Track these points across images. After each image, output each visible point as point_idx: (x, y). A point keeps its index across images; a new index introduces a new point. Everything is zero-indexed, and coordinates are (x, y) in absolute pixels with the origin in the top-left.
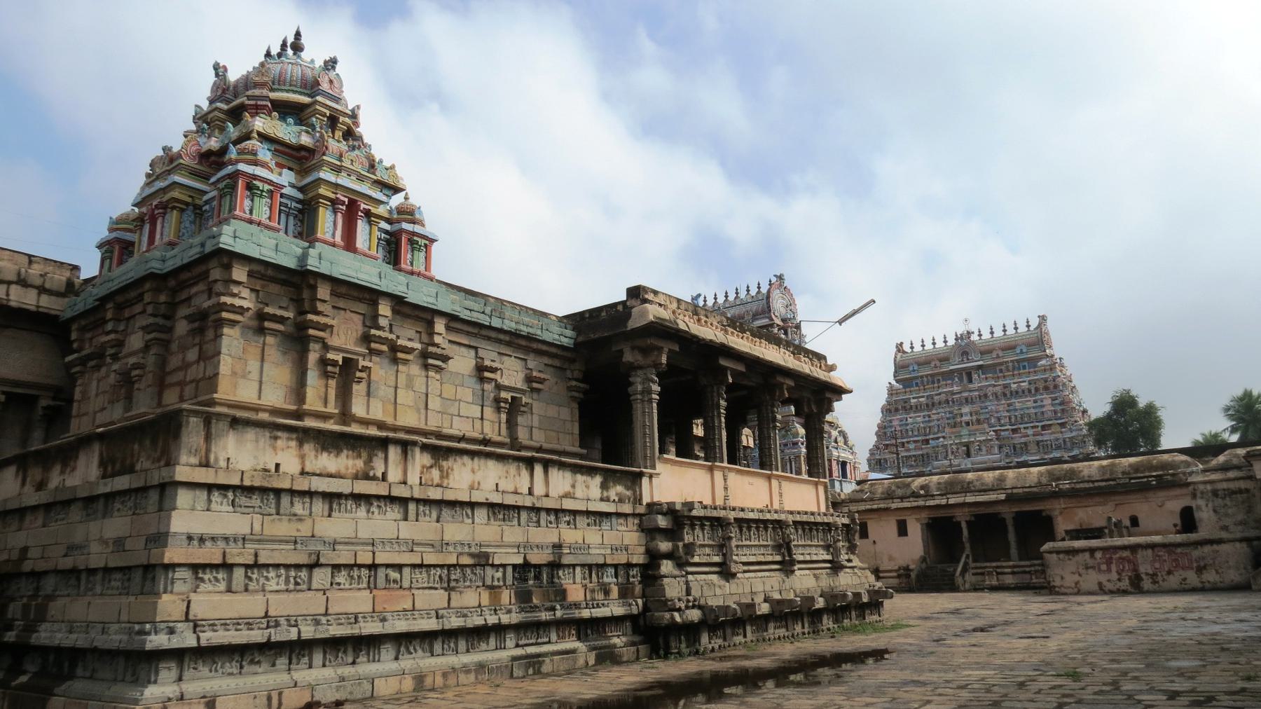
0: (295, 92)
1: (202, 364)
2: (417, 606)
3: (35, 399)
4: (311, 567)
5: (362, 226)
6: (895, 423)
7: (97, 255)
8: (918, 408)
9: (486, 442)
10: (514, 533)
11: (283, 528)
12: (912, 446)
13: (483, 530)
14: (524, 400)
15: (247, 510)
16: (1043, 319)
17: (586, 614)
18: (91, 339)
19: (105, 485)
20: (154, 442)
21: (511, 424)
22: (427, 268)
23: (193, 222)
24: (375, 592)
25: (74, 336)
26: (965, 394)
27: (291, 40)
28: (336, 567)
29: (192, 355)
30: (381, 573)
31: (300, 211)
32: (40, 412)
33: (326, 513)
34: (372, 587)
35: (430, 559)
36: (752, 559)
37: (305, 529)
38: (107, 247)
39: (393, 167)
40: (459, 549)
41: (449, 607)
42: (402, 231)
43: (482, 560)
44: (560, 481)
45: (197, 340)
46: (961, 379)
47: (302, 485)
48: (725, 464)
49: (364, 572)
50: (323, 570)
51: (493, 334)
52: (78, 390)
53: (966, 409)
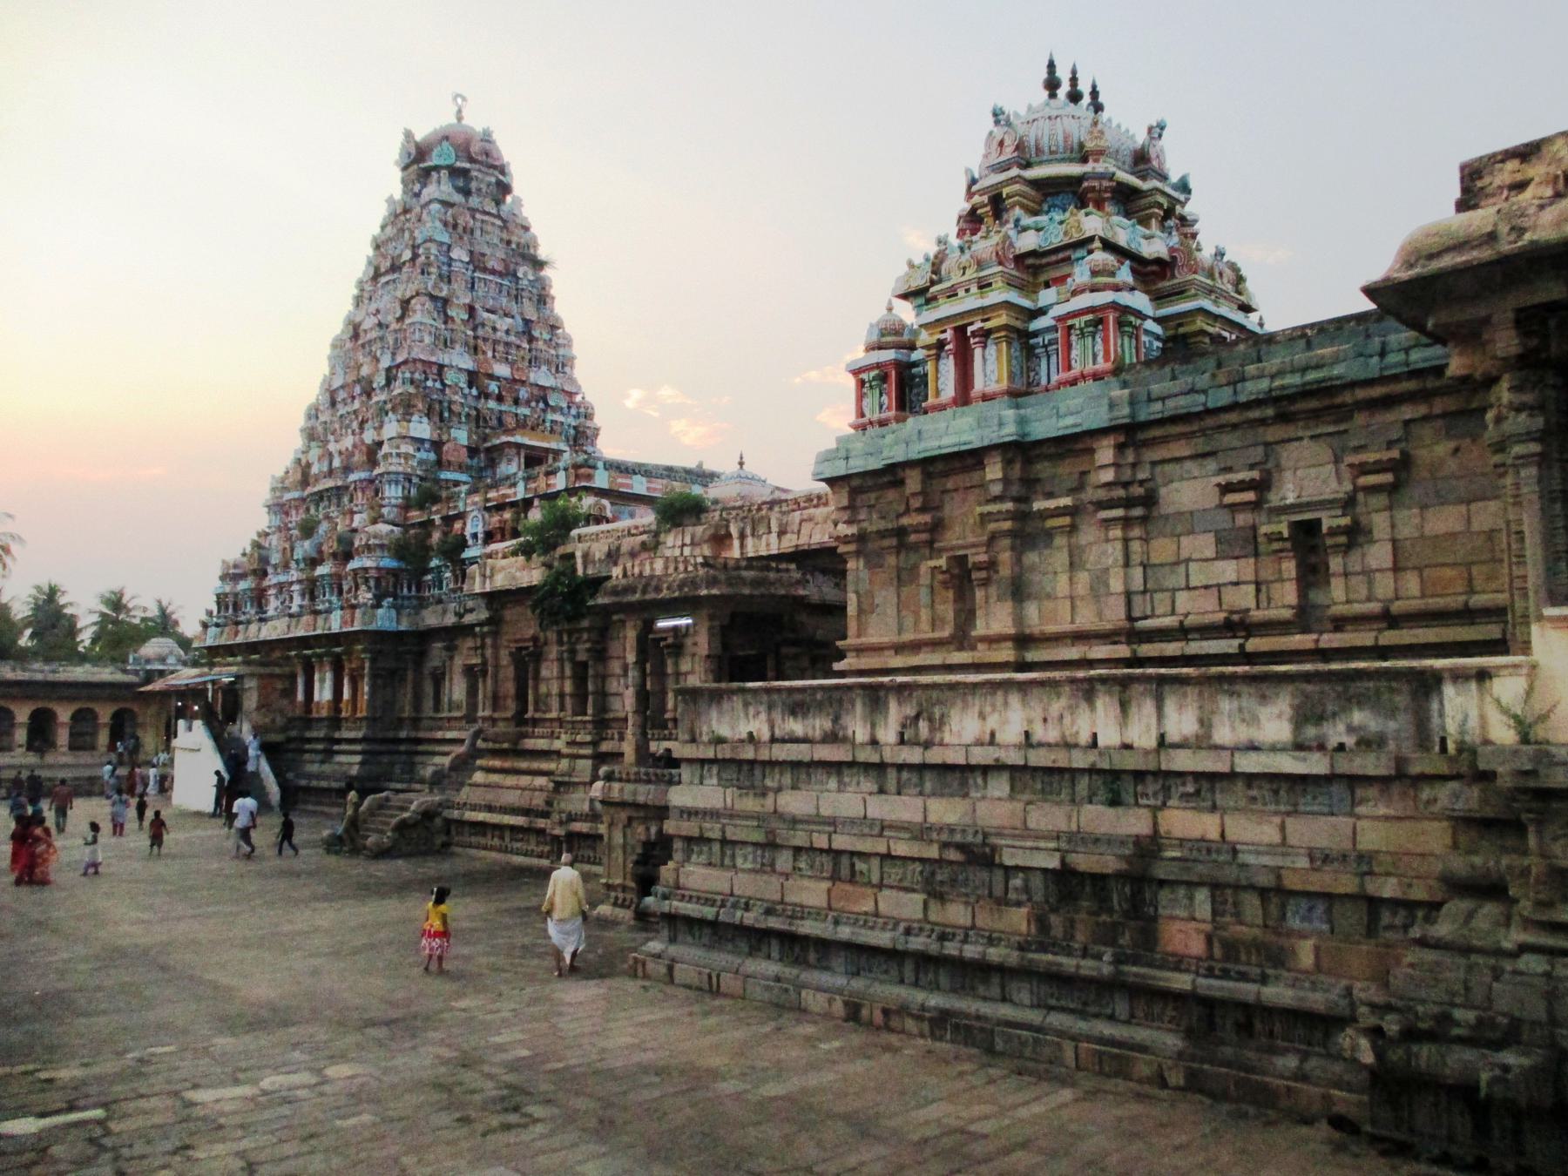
9: (1390, 620)
10: (1049, 817)
11: (750, 804)
20: (1200, 694)
28: (798, 850)
33: (696, 781)
34: (835, 877)
35: (901, 849)
40: (945, 837)
49: (825, 859)
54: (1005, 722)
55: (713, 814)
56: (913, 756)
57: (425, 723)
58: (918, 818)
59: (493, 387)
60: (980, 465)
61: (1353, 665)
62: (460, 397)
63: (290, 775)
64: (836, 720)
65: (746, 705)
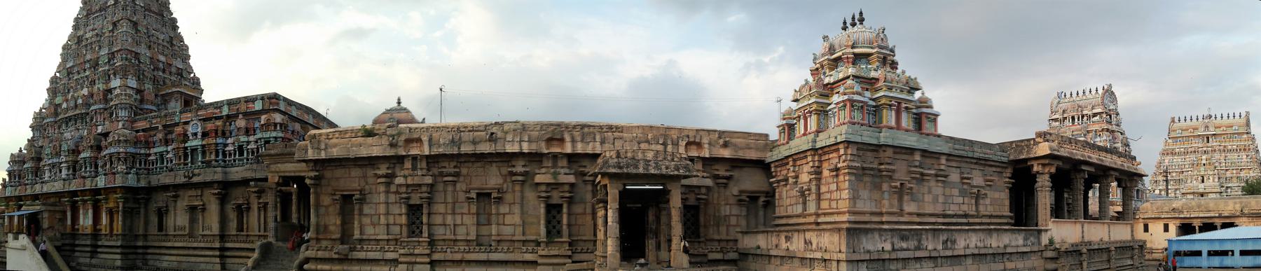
5: (904, 116)
7: (777, 130)
9: (966, 216)
14: (983, 192)
21: (977, 204)
27: (857, 17)
29: (833, 187)
38: (782, 128)
47: (894, 256)
56: (949, 253)
57: (150, 238)
59: (161, 65)
62: (147, 69)
63: (74, 264)
64: (919, 241)
65: (881, 236)
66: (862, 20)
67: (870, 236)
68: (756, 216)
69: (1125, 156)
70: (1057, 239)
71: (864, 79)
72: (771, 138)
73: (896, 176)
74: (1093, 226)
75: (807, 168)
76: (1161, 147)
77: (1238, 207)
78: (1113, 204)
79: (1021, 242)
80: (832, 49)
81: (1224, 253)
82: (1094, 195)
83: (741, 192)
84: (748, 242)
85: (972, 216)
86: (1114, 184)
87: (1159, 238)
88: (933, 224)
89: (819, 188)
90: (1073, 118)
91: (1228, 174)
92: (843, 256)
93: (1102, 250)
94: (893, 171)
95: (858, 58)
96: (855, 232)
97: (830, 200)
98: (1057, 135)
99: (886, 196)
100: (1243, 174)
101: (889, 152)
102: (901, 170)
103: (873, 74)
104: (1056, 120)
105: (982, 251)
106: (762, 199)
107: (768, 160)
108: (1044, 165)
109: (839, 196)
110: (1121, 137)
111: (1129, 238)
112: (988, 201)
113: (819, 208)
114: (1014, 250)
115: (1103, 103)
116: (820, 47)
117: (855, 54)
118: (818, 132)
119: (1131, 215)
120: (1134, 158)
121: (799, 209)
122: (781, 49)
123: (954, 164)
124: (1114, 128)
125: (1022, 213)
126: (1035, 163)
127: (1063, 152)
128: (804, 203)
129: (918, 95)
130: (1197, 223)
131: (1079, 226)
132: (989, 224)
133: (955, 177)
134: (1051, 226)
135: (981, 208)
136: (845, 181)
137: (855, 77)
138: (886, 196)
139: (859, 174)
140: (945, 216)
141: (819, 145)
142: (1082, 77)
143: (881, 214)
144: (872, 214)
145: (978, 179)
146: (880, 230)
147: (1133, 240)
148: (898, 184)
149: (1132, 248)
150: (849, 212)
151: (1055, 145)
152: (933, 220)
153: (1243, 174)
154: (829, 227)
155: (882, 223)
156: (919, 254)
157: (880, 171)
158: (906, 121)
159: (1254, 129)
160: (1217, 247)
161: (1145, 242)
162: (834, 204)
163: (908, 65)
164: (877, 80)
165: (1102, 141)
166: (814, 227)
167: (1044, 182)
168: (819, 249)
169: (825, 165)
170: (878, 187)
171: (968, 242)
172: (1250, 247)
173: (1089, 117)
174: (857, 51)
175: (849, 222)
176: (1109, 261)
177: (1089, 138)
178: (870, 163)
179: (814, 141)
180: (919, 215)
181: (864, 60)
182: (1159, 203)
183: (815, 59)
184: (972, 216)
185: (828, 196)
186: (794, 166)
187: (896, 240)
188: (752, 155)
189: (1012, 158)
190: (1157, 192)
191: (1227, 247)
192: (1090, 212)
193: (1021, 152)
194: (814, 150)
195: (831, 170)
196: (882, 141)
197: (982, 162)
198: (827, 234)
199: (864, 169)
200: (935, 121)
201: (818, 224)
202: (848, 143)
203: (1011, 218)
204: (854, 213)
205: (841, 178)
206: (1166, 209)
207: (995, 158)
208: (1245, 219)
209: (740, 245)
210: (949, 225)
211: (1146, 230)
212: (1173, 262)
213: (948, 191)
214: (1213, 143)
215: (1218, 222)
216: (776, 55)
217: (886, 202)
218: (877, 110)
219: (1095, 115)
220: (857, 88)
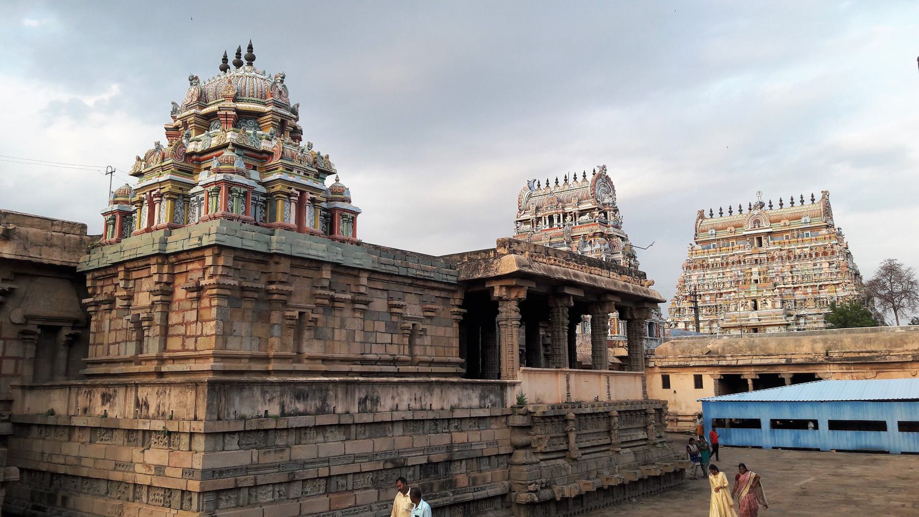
0: (253, 102)
1: (199, 323)
2: (358, 502)
3: (58, 329)
4: (290, 482)
5: (309, 211)
6: (694, 278)
7: (102, 220)
8: (714, 266)
9: (394, 362)
10: (421, 441)
11: (272, 458)
12: (707, 298)
13: (400, 440)
14: (421, 326)
15: (248, 447)
16: (825, 193)
17: (469, 496)
18: (102, 287)
19: (144, 423)
21: (411, 345)
22: (354, 235)
23: (183, 208)
24: (331, 496)
25: (89, 284)
26: (756, 257)
27: (244, 52)
29: (191, 316)
30: (333, 482)
31: (264, 202)
32: (64, 339)
35: (366, 467)
36: (588, 444)
37: (285, 456)
38: (110, 218)
39: (327, 157)
40: (383, 457)
41: (379, 501)
42: (336, 209)
43: (399, 465)
44: (453, 397)
45: (195, 305)
46: (752, 244)
47: (283, 424)
48: (568, 369)
50: (296, 484)
51: (400, 280)
52: (93, 324)
53: (755, 270)
54: (401, 400)
55: (246, 469)
56: (368, 418)
58: (370, 450)
60: (319, 269)
61: (370, 379)
64: (324, 400)
65: (264, 393)
66: (251, 59)
67: (246, 393)
68: (53, 358)
69: (630, 273)
70: (530, 398)
71: (243, 141)
72: (90, 232)
73: (294, 301)
74: (583, 378)
75: (147, 285)
76: (684, 256)
77: (820, 348)
78: (612, 344)
79: (475, 402)
80: (202, 100)
81: (801, 425)
82: (583, 333)
83: (28, 318)
84: (33, 405)
85: (404, 362)
86: (614, 315)
87: (688, 398)
88: (347, 373)
89: (166, 316)
90: (551, 218)
91: (799, 295)
92: (200, 427)
93: (598, 416)
94: (290, 294)
95: (242, 118)
96: (221, 387)
97: (185, 336)
98: (529, 244)
99: (276, 331)
100: (824, 294)
101: (285, 265)
102: (301, 292)
103: (264, 145)
104: (526, 222)
105: (419, 416)
106: (66, 332)
107: (82, 268)
108: (509, 288)
109: (201, 331)
110: (622, 244)
111: (639, 396)
112: (427, 341)
113: (164, 348)
114: (466, 414)
115: (594, 196)
116: (184, 94)
117: (236, 110)
118: (171, 227)
119: (641, 362)
120: (643, 275)
121: (130, 350)
122: (115, 88)
123: (379, 285)
124: (612, 231)
125: (478, 359)
126: (496, 285)
127: (539, 268)
128: (140, 340)
129: (329, 181)
130: (749, 375)
131: (562, 379)
132: (428, 374)
133: (379, 304)
134: (520, 377)
135: (418, 351)
136: (211, 307)
137: (236, 147)
138: (276, 331)
139: (234, 297)
140: (364, 362)
141: (171, 248)
142: (563, 157)
143: (266, 359)
144: (253, 358)
145: (413, 308)
146: (264, 383)
147: (646, 400)
148: (296, 313)
149: (646, 413)
150: (215, 356)
151: (525, 258)
152: (345, 368)
153: (824, 294)
154: (179, 379)
155: (268, 373)
156: (322, 420)
157: (269, 292)
158: (311, 220)
159: (838, 220)
160: (786, 414)
161: (665, 403)
162: (190, 344)
163: (316, 136)
164: (270, 154)
165: (594, 250)
166: (153, 379)
167: (509, 312)
168: (161, 415)
169: (180, 281)
170: (264, 318)
171: (397, 402)
172: (847, 415)
173: (574, 216)
174: (241, 106)
175: (214, 372)
176: (609, 432)
177: (575, 247)
178: (255, 280)
179: (164, 242)
180: (324, 360)
181: (251, 122)
182: (685, 343)
183: (174, 111)
184: (404, 362)
185: (181, 330)
186: (127, 280)
187: (287, 400)
188: (56, 257)
189: (462, 277)
190: (681, 326)
191: (870, 415)
192: (579, 357)
193: (476, 269)
194: (163, 257)
195: (189, 290)
196: (275, 248)
197: (420, 283)
198: (175, 392)
199: (243, 289)
200: (354, 220)
201: (161, 374)
202: (219, 248)
203: (461, 365)
204: (224, 358)
205: (205, 302)
206: (697, 352)
207: (439, 277)
208: (833, 368)
209: (16, 410)
210: (368, 376)
211: (666, 384)
212: (713, 437)
213: (369, 325)
214: (769, 246)
215: (786, 373)
216: (106, 96)
217: (275, 341)
218: (268, 201)
219: (582, 213)
220: (239, 164)
